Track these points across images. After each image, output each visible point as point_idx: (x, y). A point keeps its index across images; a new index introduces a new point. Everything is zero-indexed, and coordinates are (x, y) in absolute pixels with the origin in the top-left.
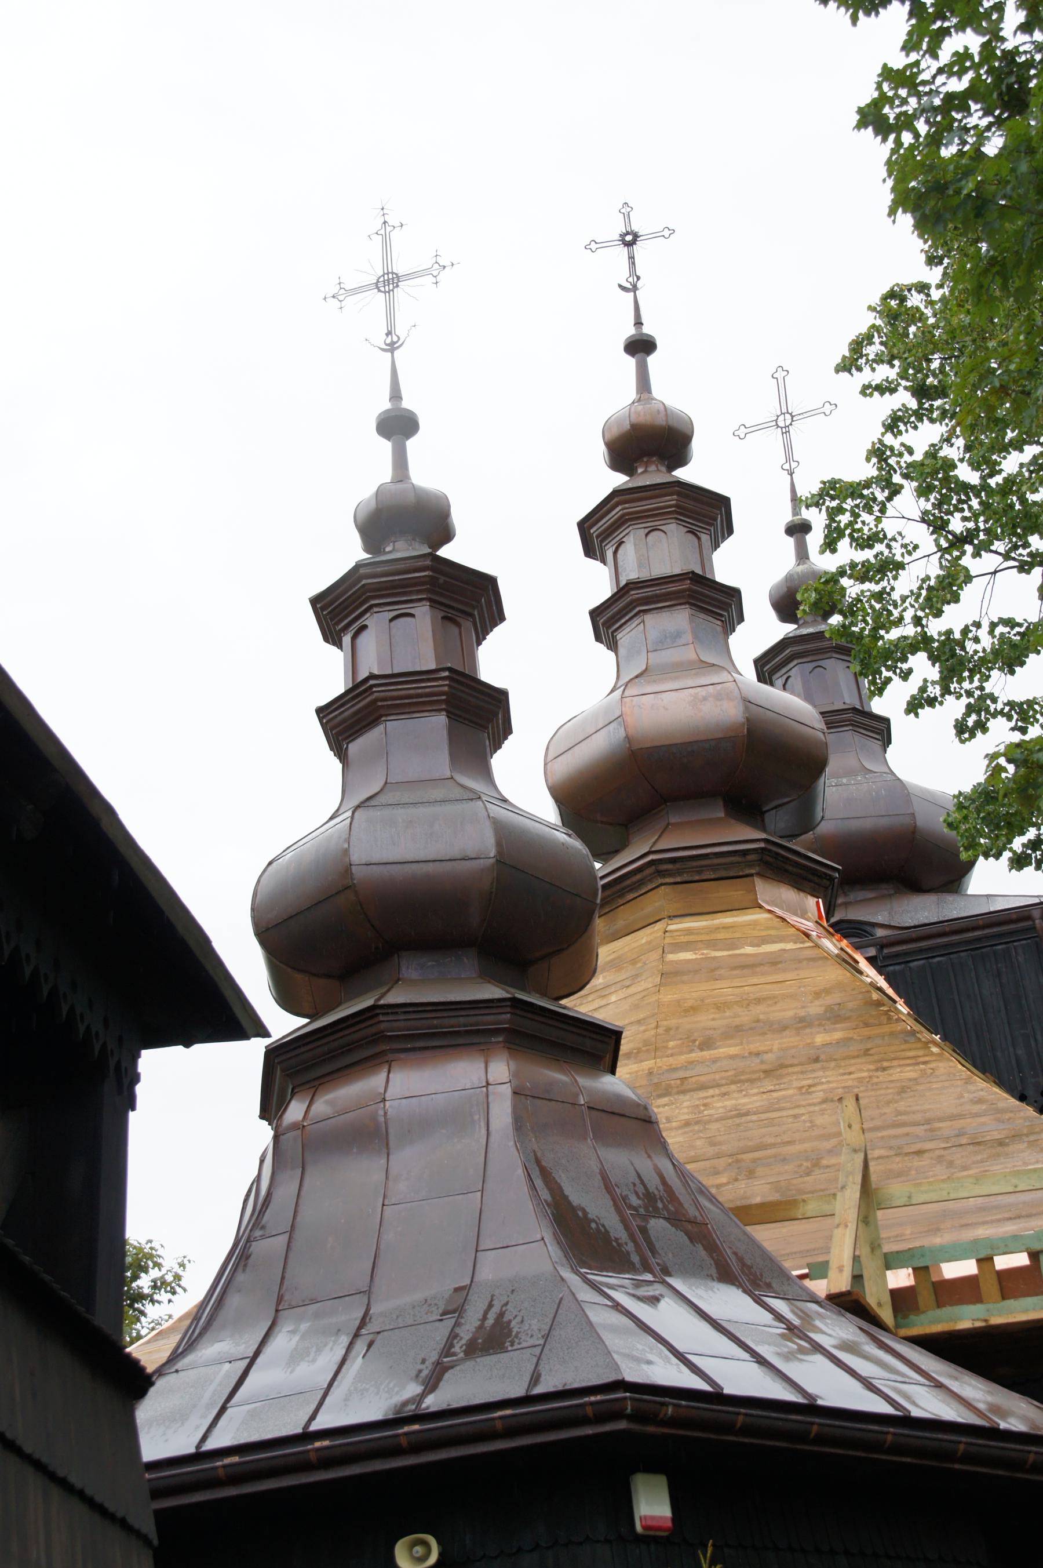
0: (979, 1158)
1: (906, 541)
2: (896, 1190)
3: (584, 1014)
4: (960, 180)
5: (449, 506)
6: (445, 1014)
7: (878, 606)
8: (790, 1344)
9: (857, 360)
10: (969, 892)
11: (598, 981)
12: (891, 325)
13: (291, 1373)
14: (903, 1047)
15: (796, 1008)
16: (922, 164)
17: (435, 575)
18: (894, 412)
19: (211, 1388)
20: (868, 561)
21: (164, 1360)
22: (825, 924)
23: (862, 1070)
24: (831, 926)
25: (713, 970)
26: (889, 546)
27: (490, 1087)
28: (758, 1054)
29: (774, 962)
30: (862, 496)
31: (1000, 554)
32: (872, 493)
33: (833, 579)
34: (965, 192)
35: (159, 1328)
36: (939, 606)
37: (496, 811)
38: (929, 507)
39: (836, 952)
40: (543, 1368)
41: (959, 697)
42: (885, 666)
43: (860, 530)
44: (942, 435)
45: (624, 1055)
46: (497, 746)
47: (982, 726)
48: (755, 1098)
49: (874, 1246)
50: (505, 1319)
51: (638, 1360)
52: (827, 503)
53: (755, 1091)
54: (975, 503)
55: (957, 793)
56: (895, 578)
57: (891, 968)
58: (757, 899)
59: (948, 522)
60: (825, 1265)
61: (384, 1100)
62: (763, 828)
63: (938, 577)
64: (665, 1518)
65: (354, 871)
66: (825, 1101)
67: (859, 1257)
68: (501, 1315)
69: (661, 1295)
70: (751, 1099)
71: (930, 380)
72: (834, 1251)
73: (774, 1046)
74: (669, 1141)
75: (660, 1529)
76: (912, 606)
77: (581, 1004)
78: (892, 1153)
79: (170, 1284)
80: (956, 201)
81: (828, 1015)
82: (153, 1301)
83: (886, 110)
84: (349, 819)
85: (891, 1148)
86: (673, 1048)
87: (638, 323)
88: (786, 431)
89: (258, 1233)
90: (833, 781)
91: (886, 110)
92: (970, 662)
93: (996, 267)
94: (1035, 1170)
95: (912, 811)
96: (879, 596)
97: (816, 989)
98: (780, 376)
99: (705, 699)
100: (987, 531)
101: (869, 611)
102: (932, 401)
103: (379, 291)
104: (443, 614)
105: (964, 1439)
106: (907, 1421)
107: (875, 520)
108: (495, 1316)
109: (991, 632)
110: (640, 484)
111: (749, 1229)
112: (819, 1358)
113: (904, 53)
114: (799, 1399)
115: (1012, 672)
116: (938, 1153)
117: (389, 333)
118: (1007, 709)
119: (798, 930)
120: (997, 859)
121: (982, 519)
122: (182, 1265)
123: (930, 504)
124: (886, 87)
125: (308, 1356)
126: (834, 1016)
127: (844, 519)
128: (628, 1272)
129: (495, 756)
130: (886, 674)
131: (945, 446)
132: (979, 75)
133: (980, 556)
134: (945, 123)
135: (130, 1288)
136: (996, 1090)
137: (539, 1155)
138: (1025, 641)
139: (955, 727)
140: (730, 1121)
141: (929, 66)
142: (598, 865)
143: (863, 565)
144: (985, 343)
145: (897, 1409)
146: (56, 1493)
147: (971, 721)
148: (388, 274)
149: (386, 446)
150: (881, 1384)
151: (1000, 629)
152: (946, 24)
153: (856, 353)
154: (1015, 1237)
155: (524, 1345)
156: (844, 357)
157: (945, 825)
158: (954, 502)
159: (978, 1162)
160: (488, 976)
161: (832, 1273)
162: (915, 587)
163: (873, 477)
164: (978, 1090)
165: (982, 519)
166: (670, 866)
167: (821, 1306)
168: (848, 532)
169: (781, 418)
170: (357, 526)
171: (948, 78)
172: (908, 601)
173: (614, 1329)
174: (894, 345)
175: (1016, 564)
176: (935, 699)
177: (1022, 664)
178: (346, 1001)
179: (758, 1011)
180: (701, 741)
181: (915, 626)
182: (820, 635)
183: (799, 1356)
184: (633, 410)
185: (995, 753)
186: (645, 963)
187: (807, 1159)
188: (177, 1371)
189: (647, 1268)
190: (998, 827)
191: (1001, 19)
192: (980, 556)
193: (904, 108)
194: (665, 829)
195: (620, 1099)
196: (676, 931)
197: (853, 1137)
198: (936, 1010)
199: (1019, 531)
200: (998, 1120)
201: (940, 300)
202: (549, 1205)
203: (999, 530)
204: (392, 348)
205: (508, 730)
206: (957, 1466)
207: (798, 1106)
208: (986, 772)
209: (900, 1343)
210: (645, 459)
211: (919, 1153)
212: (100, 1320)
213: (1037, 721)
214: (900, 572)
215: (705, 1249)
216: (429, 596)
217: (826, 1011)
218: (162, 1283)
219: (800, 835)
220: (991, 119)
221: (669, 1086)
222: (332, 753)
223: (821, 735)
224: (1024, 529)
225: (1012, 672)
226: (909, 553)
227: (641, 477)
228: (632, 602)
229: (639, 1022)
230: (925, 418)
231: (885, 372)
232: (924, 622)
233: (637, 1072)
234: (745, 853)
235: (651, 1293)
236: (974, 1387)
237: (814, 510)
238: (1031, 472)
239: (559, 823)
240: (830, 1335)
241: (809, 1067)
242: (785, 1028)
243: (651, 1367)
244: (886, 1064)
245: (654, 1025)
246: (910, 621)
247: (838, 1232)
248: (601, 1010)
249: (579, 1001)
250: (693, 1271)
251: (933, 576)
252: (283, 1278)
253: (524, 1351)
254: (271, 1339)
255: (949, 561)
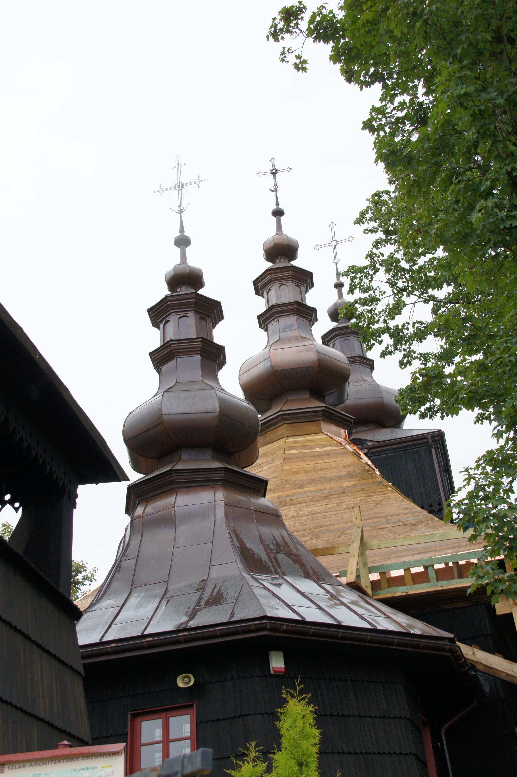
0: (406, 530)
1: (381, 290)
2: (374, 543)
3: (254, 474)
4: (402, 150)
5: (202, 274)
6: (198, 473)
7: (370, 315)
8: (331, 602)
9: (362, 219)
10: (404, 428)
11: (259, 461)
12: (375, 206)
13: (137, 612)
14: (377, 488)
15: (336, 472)
16: (388, 143)
17: (197, 301)
18: (377, 240)
19: (106, 617)
20: (366, 297)
21: (88, 606)
22: (348, 440)
23: (362, 496)
24: (350, 440)
25: (304, 457)
26: (374, 292)
27: (216, 502)
28: (321, 490)
29: (328, 454)
30: (364, 272)
31: (417, 296)
32: (368, 271)
33: (352, 305)
34: (404, 154)
35: (85, 595)
36: (393, 315)
37: (220, 394)
38: (390, 277)
39: (352, 450)
40: (236, 611)
41: (401, 351)
42: (372, 339)
43: (363, 286)
44: (395, 249)
45: (269, 490)
46: (220, 368)
47: (409, 363)
48: (320, 507)
49: (365, 564)
50: (221, 592)
51: (272, 608)
52: (351, 275)
53: (320, 504)
54: (407, 276)
55: (399, 389)
56: (377, 304)
57: (373, 457)
58: (321, 430)
59: (397, 283)
60: (346, 571)
61: (174, 507)
62: (324, 402)
63: (393, 304)
64: (282, 668)
65: (163, 417)
66: (346, 509)
67: (359, 568)
68: (219, 590)
69: (282, 583)
70: (318, 508)
71: (390, 228)
72: (349, 566)
73: (328, 487)
74: (286, 524)
75: (280, 672)
76: (383, 315)
77: (252, 470)
78: (372, 529)
79: (90, 578)
80: (400, 158)
81: (348, 475)
82: (83, 584)
83: (374, 123)
84: (162, 397)
85: (372, 527)
86: (288, 488)
87: (277, 204)
88: (334, 247)
89: (124, 558)
90: (352, 384)
91: (374, 123)
92: (405, 338)
93: (416, 183)
94: (427, 535)
95: (381, 396)
96: (370, 311)
97: (344, 465)
98: (332, 226)
99: (302, 351)
100: (412, 287)
101: (366, 317)
102: (391, 236)
103: (176, 190)
104: (199, 316)
105: (397, 637)
106: (376, 631)
107: (369, 282)
108: (217, 591)
109: (413, 326)
110: (278, 267)
111: (316, 558)
112: (343, 607)
113: (380, 102)
114: (335, 623)
115: (421, 342)
116: (390, 528)
117: (180, 206)
118: (419, 356)
119: (337, 442)
120: (415, 415)
121: (410, 282)
122: (95, 571)
123: (390, 276)
124: (373, 114)
125: (144, 606)
126: (351, 476)
127: (357, 281)
128: (269, 575)
129: (219, 372)
130: (372, 342)
131: (396, 253)
132: (409, 112)
133: (409, 296)
134: (396, 128)
135: (74, 579)
136: (413, 504)
137: (235, 529)
138: (426, 330)
139: (399, 363)
140: (310, 516)
141: (390, 107)
142: (259, 416)
143: (364, 299)
144: (412, 214)
145: (372, 626)
146: (45, 656)
147: (405, 361)
148: (179, 183)
149: (178, 250)
150: (368, 617)
151: (417, 325)
152: (396, 92)
153: (362, 217)
154: (419, 561)
155: (228, 602)
156: (357, 218)
157: (395, 401)
158: (399, 275)
159: (405, 532)
160: (215, 458)
161: (348, 575)
162: (384, 308)
163: (368, 265)
164: (406, 504)
165: (410, 282)
166: (288, 417)
167: (344, 587)
168: (358, 286)
169: (333, 242)
170: (166, 281)
171: (397, 112)
172: (382, 313)
173: (263, 596)
174: (377, 214)
175: (423, 300)
176: (392, 352)
177: (425, 339)
178: (160, 468)
179: (321, 473)
180: (300, 368)
181: (384, 323)
182: (347, 327)
183: (335, 606)
184: (275, 238)
185: (415, 372)
186: (277, 455)
187: (339, 531)
188: (92, 611)
189: (277, 573)
190: (415, 402)
191: (417, 90)
192: (409, 296)
193: (381, 122)
194: (286, 402)
195: (267, 507)
196: (290, 442)
197: (358, 522)
198: (390, 474)
199: (424, 287)
200: (413, 516)
201: (394, 197)
202: (238, 548)
203: (417, 287)
204: (181, 212)
205: (224, 362)
206: (394, 647)
207: (337, 510)
208: (411, 379)
209: (374, 601)
210: (280, 257)
211: (383, 528)
212: (62, 590)
213: (431, 361)
214: (379, 302)
215: (299, 565)
216: (194, 309)
217: (348, 473)
218: (87, 578)
219: (339, 405)
220: (413, 127)
221: (286, 502)
222: (155, 370)
223: (347, 366)
224: (426, 287)
225: (421, 342)
226: (382, 295)
227: (278, 264)
228: (274, 312)
229: (275, 477)
230: (388, 243)
231: (373, 225)
232: (388, 322)
233: (274, 497)
234: (317, 411)
235: (278, 583)
236: (402, 618)
237: (345, 277)
238: (429, 265)
239: (244, 399)
240: (347, 598)
241: (341, 495)
242: (332, 480)
243: (278, 611)
244: (370, 494)
245: (281, 479)
246: (382, 321)
247: (351, 559)
248: (260, 473)
249: (251, 469)
250: (293, 574)
251: (391, 304)
252: (134, 576)
253: (228, 604)
254: (129, 599)
255: (397, 298)
